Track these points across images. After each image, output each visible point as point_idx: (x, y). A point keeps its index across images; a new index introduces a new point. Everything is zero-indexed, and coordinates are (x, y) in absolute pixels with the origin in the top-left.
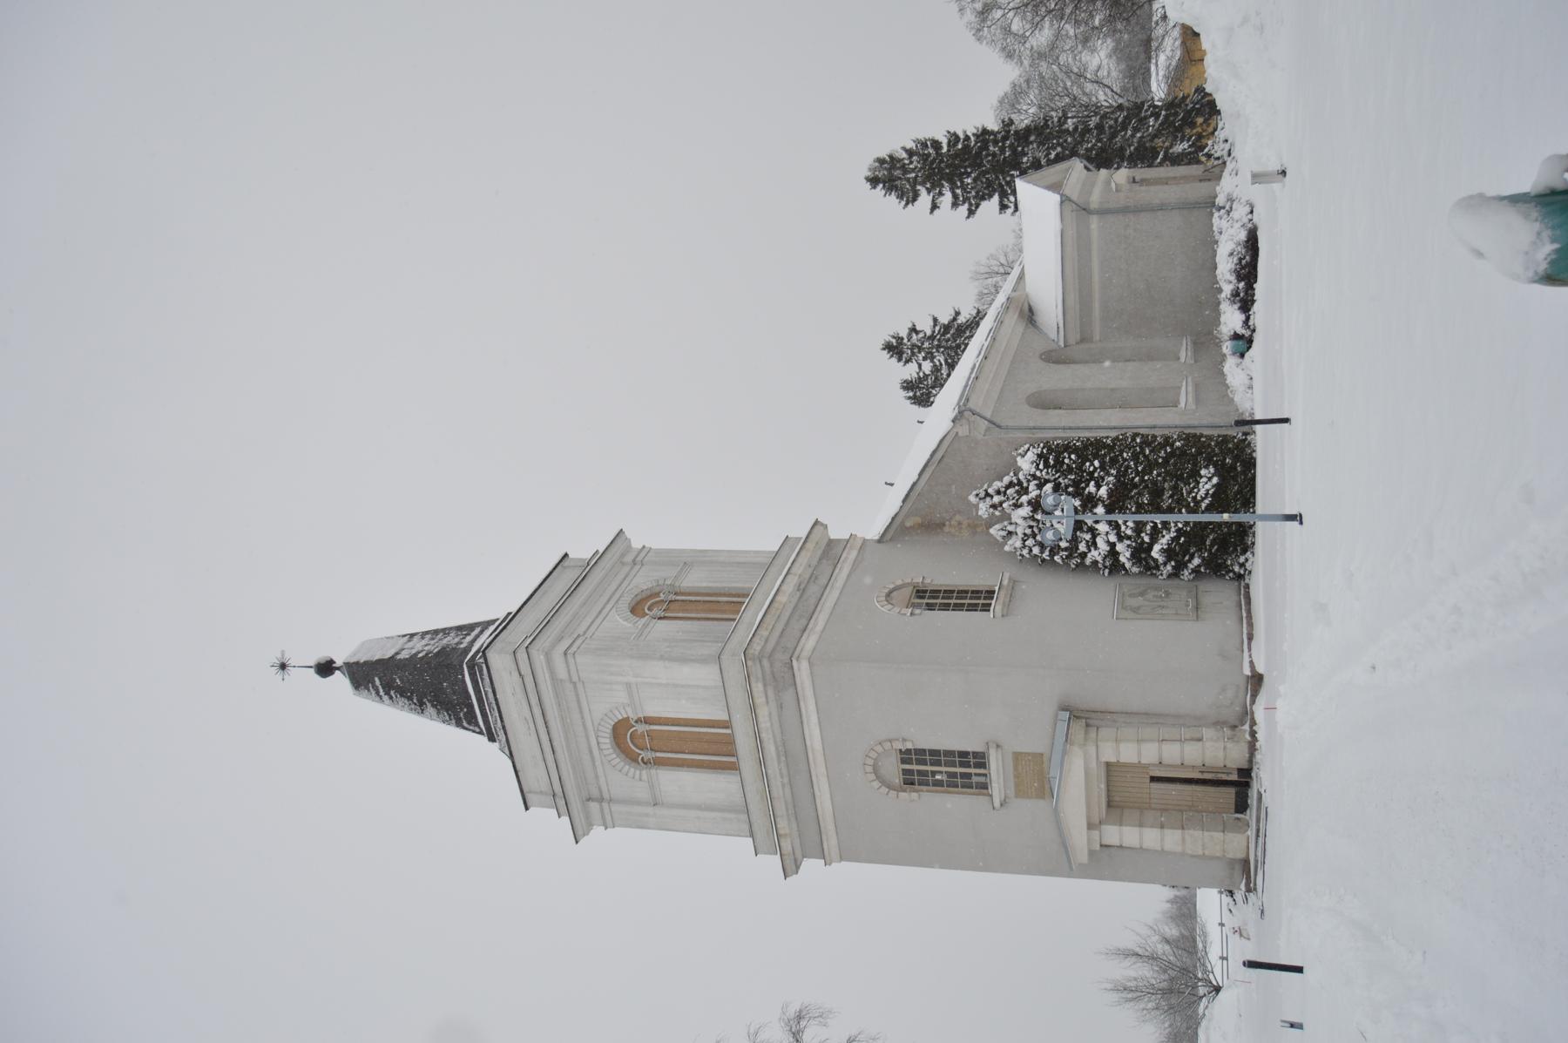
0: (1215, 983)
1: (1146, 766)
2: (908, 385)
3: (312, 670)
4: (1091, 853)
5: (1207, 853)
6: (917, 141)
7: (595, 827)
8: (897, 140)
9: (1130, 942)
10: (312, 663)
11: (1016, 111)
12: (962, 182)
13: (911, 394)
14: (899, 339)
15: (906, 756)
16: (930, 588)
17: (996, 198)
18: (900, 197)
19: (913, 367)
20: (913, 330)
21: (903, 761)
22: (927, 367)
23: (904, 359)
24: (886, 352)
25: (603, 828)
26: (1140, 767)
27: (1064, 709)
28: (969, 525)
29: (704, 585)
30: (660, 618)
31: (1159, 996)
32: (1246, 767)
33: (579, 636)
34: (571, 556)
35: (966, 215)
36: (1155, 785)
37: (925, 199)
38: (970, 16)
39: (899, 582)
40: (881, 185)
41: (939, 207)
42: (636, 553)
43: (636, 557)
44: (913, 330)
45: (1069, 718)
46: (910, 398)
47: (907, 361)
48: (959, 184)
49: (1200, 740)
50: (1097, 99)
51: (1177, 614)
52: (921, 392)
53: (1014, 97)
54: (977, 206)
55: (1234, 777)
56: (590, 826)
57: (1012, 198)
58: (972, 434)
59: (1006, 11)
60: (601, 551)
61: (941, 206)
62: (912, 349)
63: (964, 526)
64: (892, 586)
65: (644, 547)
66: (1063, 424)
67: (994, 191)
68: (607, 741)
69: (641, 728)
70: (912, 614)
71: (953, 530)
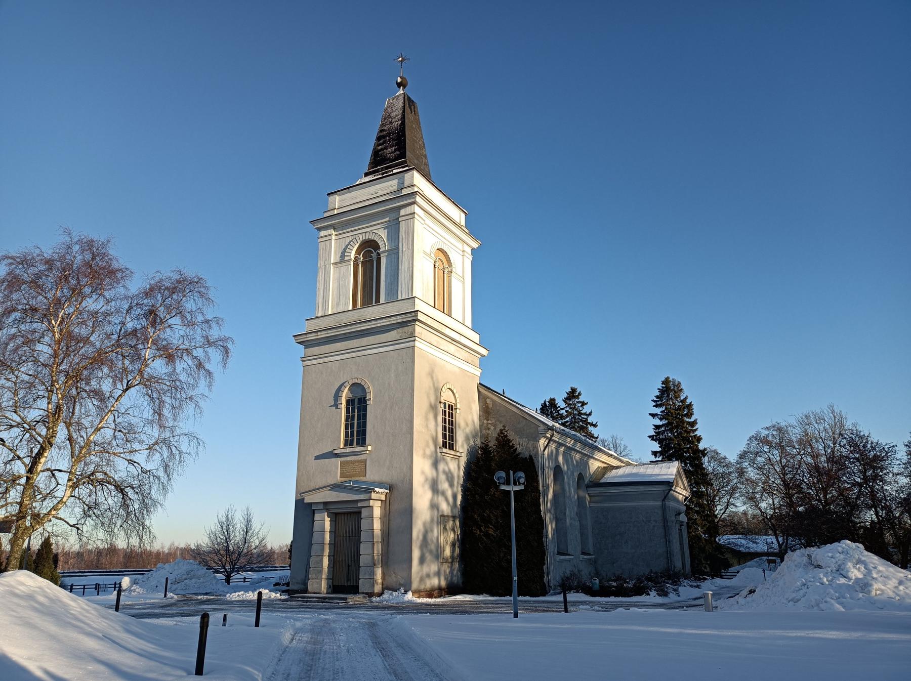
0: (232, 575)
2: (552, 401)
4: (310, 504)
5: (311, 569)
8: (689, 393)
9: (256, 526)
11: (710, 459)
12: (668, 430)
13: (547, 403)
14: (578, 397)
17: (660, 449)
19: (562, 405)
20: (583, 404)
21: (360, 400)
28: (488, 434)
31: (225, 545)
33: (424, 221)
41: (654, 418)
44: (583, 404)
52: (549, 408)
53: (721, 461)
54: (655, 440)
57: (660, 459)
59: (768, 454)
61: (655, 420)
63: (487, 431)
64: (455, 392)
68: (371, 237)
69: (374, 255)
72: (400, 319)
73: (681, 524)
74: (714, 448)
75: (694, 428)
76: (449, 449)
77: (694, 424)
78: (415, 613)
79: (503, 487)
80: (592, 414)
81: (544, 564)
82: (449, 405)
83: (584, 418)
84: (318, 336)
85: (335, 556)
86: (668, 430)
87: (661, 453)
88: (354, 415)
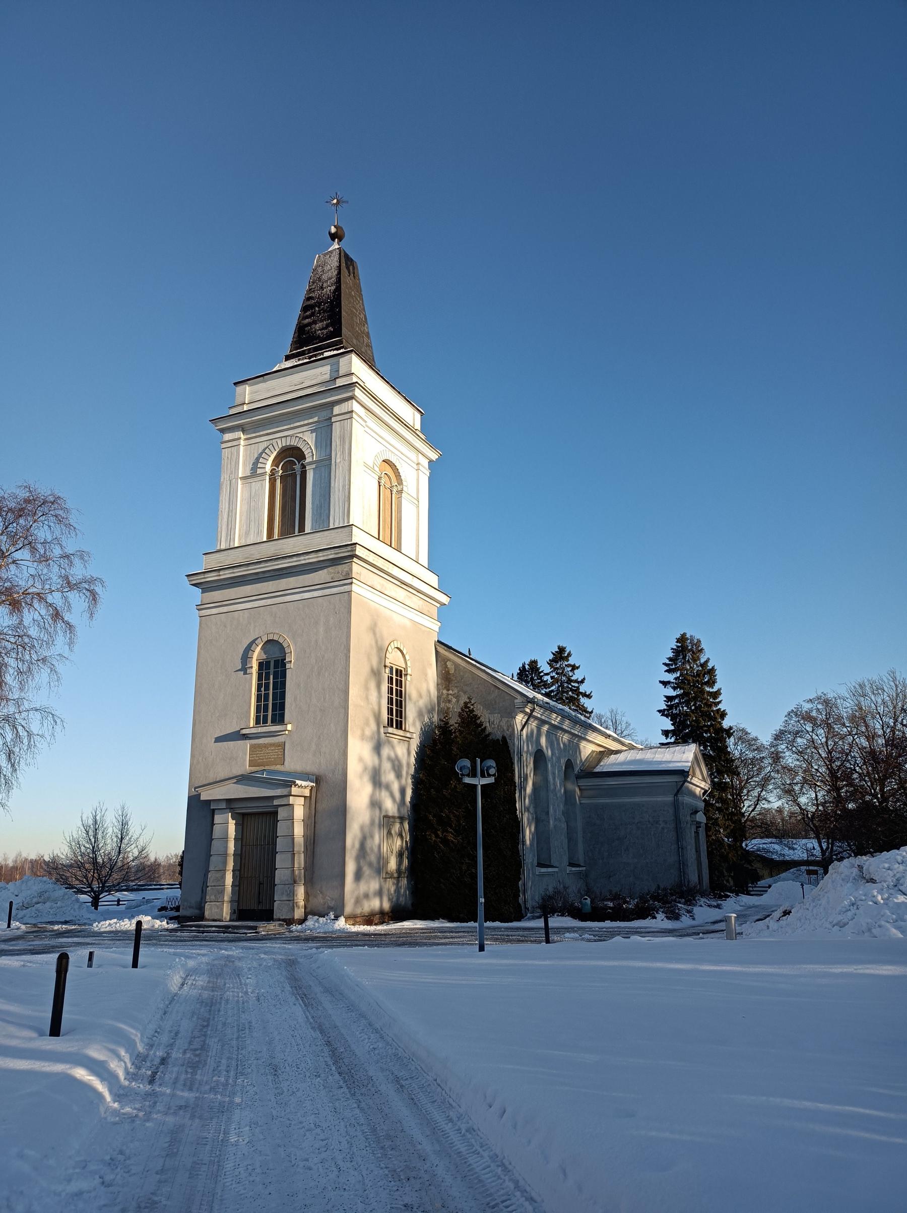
4: (208, 802)
5: (209, 889)
6: (712, 670)
9: (134, 830)
13: (527, 667)
14: (567, 658)
20: (574, 668)
21: (276, 662)
28: (448, 708)
31: (91, 856)
33: (366, 422)
38: (807, 706)
41: (665, 687)
44: (574, 668)
47: (551, 666)
50: (745, 800)
53: (744, 737)
54: (667, 716)
58: (516, 710)
59: (811, 734)
64: (405, 652)
68: (294, 442)
69: (297, 467)
72: (332, 554)
73: (698, 825)
75: (717, 700)
76: (397, 728)
77: (717, 694)
79: (467, 780)
81: (520, 879)
82: (397, 670)
83: (574, 687)
84: (220, 575)
86: (683, 703)
87: (674, 733)
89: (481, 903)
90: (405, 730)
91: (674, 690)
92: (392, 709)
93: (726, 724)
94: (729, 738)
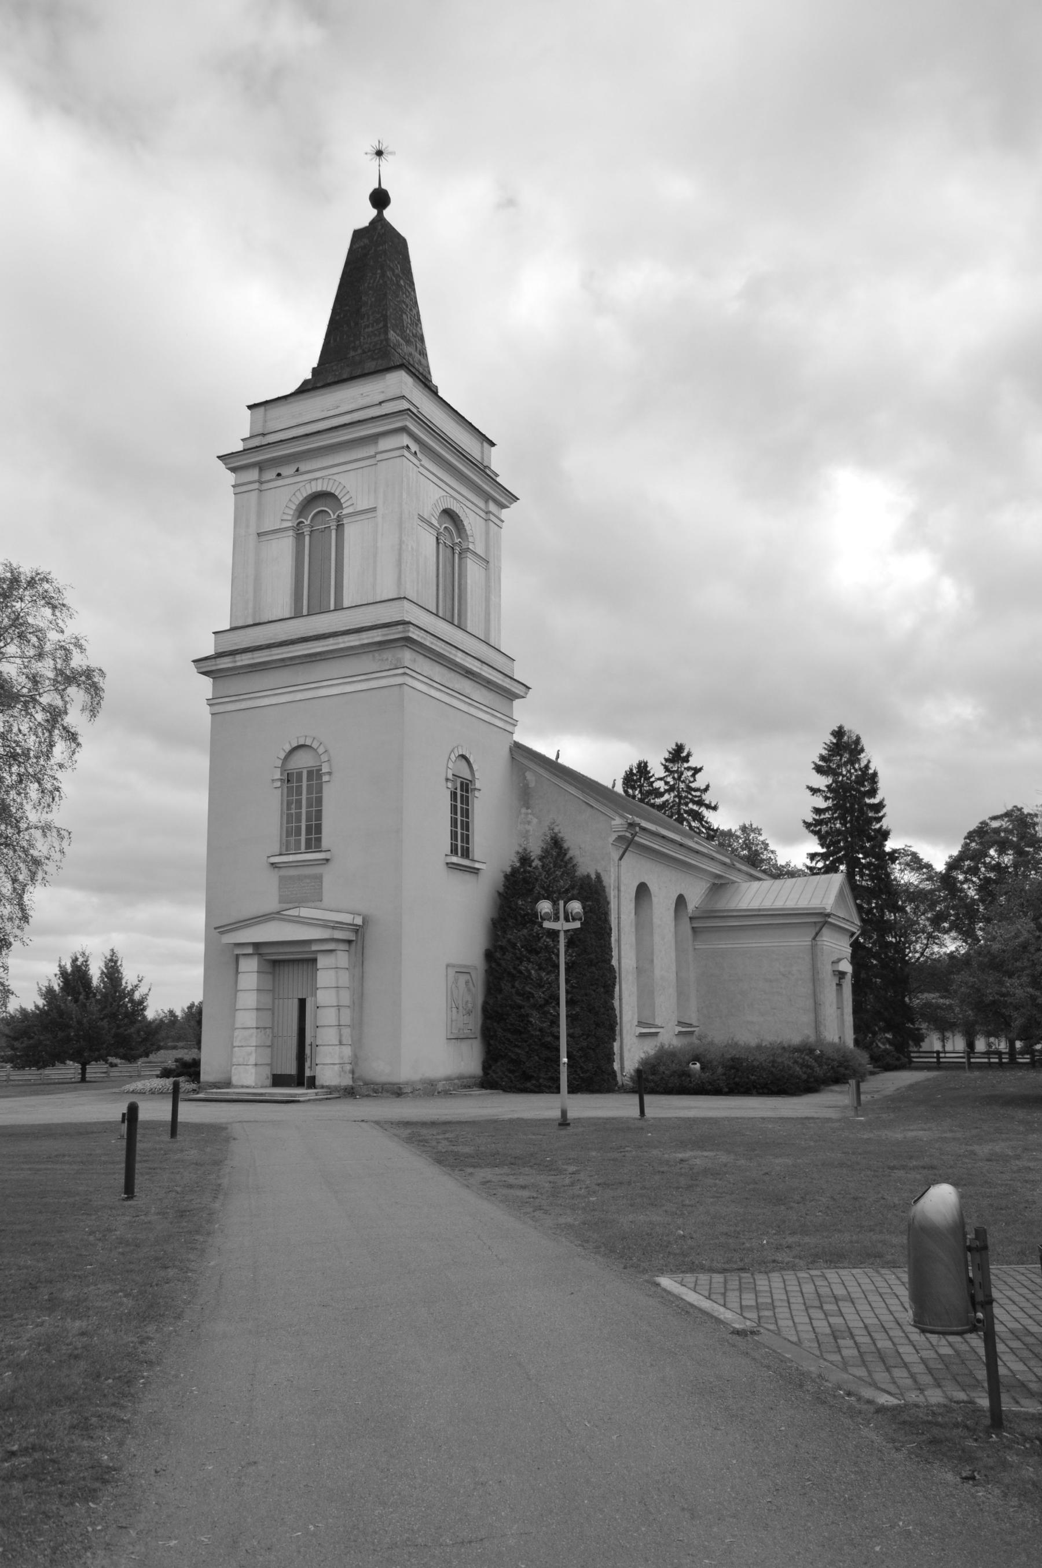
1: (314, 994)
2: (643, 768)
3: (377, 186)
6: (875, 774)
7: (234, 475)
10: (384, 186)
12: (836, 819)
14: (686, 759)
15: (315, 774)
16: (470, 795)
18: (822, 758)
20: (697, 771)
22: (660, 785)
23: (667, 764)
24: (674, 747)
25: (234, 484)
26: (314, 989)
27: (365, 920)
28: (527, 831)
29: (469, 581)
30: (437, 539)
32: (317, 1083)
34: (493, 449)
35: (806, 821)
36: (295, 1004)
37: (822, 782)
39: (475, 767)
40: (835, 741)
41: (813, 795)
42: (497, 514)
43: (494, 514)
44: (697, 771)
45: (356, 925)
46: (631, 770)
47: (667, 769)
48: (836, 815)
49: (341, 1044)
51: (452, 1021)
55: (308, 1073)
56: (233, 470)
60: (498, 479)
62: (677, 771)
64: (472, 761)
65: (503, 521)
66: (623, 917)
67: (828, 847)
70: (447, 780)
71: (523, 816)
72: (378, 636)
73: (842, 975)
74: (913, 849)
75: (880, 814)
76: (462, 855)
77: (880, 806)
78: (372, 1084)
79: (547, 925)
80: (710, 788)
81: (614, 1040)
83: (696, 796)
85: (276, 1028)
86: (836, 819)
87: (824, 856)
88: (307, 808)
89: (564, 1063)
90: (473, 860)
91: (826, 801)
92: (456, 832)
93: (889, 846)
94: (893, 862)
